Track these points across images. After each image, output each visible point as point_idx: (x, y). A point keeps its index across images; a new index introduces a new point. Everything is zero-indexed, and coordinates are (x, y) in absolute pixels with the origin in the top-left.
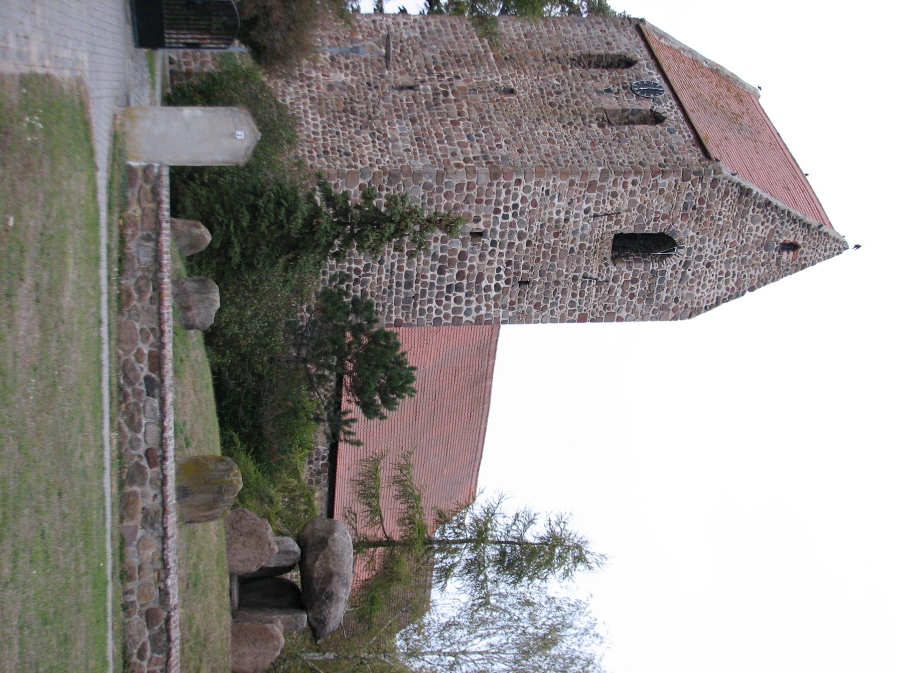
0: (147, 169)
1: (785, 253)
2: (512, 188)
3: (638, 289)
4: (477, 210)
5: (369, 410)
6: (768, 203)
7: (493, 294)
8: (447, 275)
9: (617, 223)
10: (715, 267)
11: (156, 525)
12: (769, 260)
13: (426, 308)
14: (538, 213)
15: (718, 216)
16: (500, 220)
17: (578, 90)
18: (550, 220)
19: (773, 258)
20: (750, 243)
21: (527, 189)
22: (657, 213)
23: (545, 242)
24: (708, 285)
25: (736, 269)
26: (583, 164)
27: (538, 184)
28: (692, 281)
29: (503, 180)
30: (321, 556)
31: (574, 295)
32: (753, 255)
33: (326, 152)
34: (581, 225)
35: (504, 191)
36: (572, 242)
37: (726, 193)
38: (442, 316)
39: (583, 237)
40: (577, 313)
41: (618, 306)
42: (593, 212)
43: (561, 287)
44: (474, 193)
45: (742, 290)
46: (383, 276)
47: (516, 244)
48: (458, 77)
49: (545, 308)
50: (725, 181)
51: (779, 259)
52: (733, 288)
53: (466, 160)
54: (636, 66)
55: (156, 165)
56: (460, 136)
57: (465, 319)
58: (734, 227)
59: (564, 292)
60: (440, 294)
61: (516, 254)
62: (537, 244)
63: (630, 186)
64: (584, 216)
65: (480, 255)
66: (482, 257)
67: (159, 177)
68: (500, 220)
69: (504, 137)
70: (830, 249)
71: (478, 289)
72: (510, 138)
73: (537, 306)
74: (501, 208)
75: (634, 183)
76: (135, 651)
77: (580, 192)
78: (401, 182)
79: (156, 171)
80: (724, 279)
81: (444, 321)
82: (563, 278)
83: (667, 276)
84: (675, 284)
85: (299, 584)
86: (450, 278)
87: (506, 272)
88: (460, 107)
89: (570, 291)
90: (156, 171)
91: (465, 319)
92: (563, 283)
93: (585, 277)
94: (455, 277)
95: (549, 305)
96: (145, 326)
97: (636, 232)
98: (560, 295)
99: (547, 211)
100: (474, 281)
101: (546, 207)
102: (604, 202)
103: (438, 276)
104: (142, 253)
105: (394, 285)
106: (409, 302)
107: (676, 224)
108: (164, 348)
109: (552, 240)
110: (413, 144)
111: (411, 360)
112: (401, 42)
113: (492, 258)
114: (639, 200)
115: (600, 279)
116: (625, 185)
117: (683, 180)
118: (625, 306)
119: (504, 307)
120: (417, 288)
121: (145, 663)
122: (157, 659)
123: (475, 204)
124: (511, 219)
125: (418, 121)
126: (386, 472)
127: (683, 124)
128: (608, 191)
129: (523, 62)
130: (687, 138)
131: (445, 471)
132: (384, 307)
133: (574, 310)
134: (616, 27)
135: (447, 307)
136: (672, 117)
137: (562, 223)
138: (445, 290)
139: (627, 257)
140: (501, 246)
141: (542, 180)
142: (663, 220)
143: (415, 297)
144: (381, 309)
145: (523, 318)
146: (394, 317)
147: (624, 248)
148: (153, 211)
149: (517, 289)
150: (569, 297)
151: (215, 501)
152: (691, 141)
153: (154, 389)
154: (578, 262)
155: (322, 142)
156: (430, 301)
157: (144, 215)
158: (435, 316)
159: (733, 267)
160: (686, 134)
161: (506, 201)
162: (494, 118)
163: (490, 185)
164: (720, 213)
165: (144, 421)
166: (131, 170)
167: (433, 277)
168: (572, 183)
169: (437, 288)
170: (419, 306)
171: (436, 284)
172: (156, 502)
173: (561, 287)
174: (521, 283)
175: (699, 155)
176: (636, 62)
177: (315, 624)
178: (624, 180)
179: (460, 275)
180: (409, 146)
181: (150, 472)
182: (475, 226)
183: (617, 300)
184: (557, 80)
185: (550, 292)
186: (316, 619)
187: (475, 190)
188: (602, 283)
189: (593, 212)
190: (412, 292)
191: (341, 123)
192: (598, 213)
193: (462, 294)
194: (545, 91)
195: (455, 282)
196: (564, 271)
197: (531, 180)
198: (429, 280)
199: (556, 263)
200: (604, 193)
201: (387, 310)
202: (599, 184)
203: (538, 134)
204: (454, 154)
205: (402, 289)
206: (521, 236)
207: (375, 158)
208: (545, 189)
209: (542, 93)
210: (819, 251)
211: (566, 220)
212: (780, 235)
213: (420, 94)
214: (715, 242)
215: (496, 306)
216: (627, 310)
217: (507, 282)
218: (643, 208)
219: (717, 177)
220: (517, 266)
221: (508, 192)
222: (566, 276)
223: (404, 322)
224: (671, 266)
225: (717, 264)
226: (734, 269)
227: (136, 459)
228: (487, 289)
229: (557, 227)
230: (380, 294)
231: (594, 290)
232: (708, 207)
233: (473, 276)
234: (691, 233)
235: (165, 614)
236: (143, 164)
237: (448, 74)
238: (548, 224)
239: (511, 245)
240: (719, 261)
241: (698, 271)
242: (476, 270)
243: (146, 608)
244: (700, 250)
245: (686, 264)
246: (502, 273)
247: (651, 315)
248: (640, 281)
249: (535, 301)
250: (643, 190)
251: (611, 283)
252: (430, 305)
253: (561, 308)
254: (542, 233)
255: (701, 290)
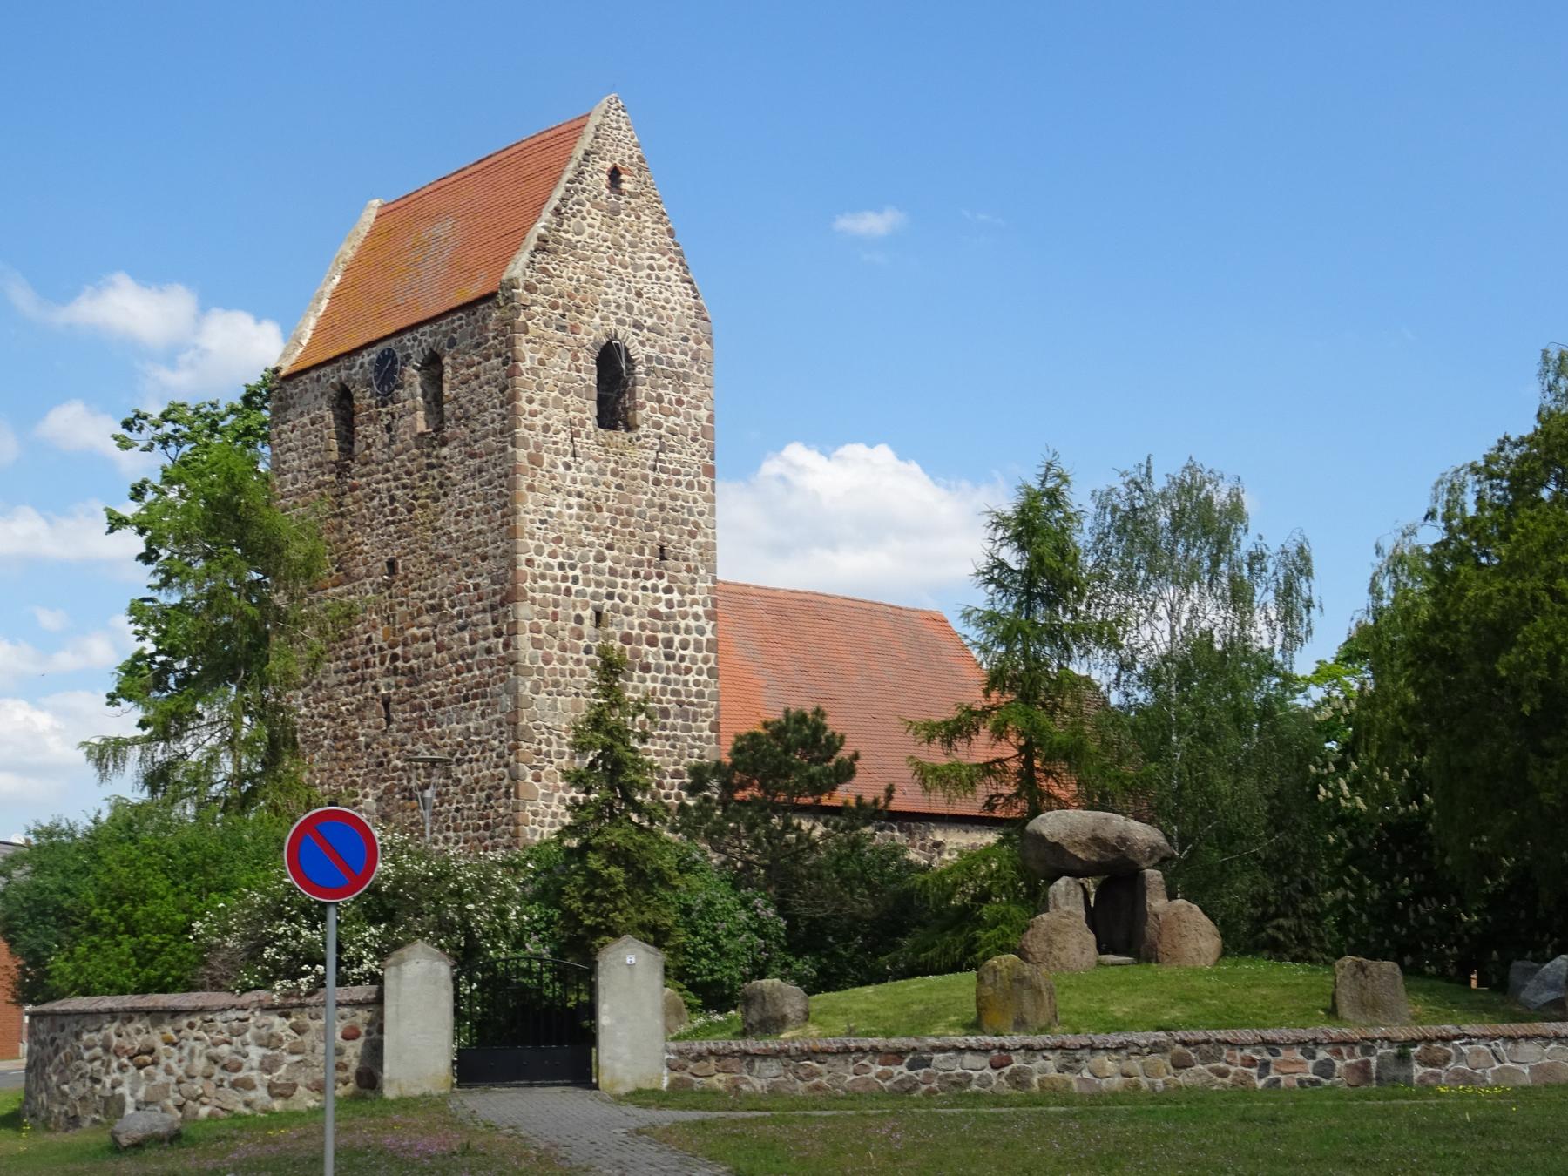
0: (672, 1067)
1: (624, 186)
2: (537, 571)
3: (670, 394)
4: (567, 619)
5: (846, 772)
6: (557, 211)
7: (676, 596)
8: (651, 660)
9: (583, 424)
10: (641, 285)
11: (1078, 1056)
12: (633, 209)
13: (694, 689)
14: (570, 536)
15: (574, 283)
16: (579, 587)
17: (387, 471)
18: (579, 518)
19: (629, 203)
20: (610, 236)
21: (539, 551)
22: (570, 369)
23: (608, 524)
24: (666, 294)
25: (645, 256)
26: (502, 472)
27: (532, 536)
28: (660, 318)
29: (527, 584)
30: (1071, 851)
31: (679, 484)
32: (626, 231)
33: (487, 827)
34: (585, 475)
35: (541, 582)
36: (609, 487)
37: (544, 270)
38: (705, 667)
39: (602, 472)
40: (702, 479)
41: (693, 422)
42: (569, 459)
43: (668, 502)
44: (544, 624)
45: (673, 247)
46: (653, 748)
47: (611, 564)
48: (369, 640)
49: (696, 524)
50: (528, 273)
51: (631, 195)
52: (670, 260)
53: (498, 634)
54: (350, 385)
55: (667, 1056)
56: (462, 640)
57: (709, 635)
58: (588, 259)
59: (674, 497)
60: (677, 670)
61: (623, 564)
62: (610, 535)
63: (535, 406)
64: (573, 470)
65: (626, 614)
66: (628, 612)
67: (679, 1053)
68: (579, 587)
69: (461, 580)
70: (617, 122)
71: (670, 617)
72: (462, 573)
73: (692, 535)
74: (563, 586)
75: (530, 401)
76: (1219, 1080)
77: (543, 476)
78: (531, 724)
79: (673, 1057)
80: (657, 272)
81: (712, 664)
82: (656, 500)
83: (654, 352)
84: (664, 341)
85: (1101, 878)
86: (656, 655)
87: (647, 578)
88: (415, 638)
89: (674, 489)
90: (673, 1057)
91: (709, 635)
92: (662, 500)
93: (654, 469)
94: (654, 649)
95: (692, 518)
96: (851, 1069)
97: (595, 397)
98: (679, 503)
99: (568, 522)
100: (659, 623)
101: (563, 524)
102: (555, 443)
103: (653, 673)
104: (767, 1073)
105: (664, 733)
106: (687, 712)
107: (585, 341)
108: (876, 1047)
109: (606, 514)
110: (473, 707)
111: (776, 715)
112: (312, 717)
113: (630, 598)
114: (553, 394)
115: (657, 447)
116: (533, 414)
117: (526, 332)
118: (692, 412)
119: (693, 581)
120: (669, 702)
121: (1233, 1069)
122: (1228, 1055)
123: (558, 622)
124: (578, 572)
125: (438, 697)
126: (936, 755)
127: (441, 326)
128: (541, 438)
129: (344, 546)
130: (463, 322)
131: (903, 656)
132: (693, 747)
133: (699, 482)
134: (286, 409)
135: (694, 660)
136: (430, 340)
137: (584, 501)
138: (671, 663)
139: (625, 410)
140: (613, 585)
141: (527, 530)
142: (578, 360)
143: (680, 704)
144: (696, 751)
145: (708, 552)
146: (707, 733)
147: (614, 412)
148: (718, 1061)
149: (670, 563)
150: (682, 490)
151: (1031, 987)
152: (468, 316)
153: (923, 1060)
154: (634, 478)
155: (471, 833)
156: (686, 683)
157: (724, 1070)
158: (705, 677)
159: (641, 259)
160: (457, 324)
161: (554, 579)
162: (431, 591)
163: (533, 601)
164: (570, 279)
165: (960, 1071)
166: (674, 1084)
167: (654, 680)
168: (531, 488)
169: (668, 673)
170: (693, 699)
171: (664, 675)
172: (1051, 1057)
173: (668, 502)
174: (663, 558)
175: (490, 308)
176: (342, 384)
177: (1156, 860)
178: (526, 416)
179: (652, 642)
180: (478, 711)
181: (1018, 1062)
182: (587, 622)
183: (685, 423)
184: (372, 499)
185: (674, 517)
186: (1150, 858)
187: (540, 622)
188: (663, 444)
189: (569, 459)
190: (673, 708)
191: (441, 805)
192: (570, 450)
193: (677, 639)
194: (390, 518)
195: (661, 648)
196: (646, 497)
197: (527, 545)
198: (659, 686)
199: (637, 509)
200: (544, 442)
201: (698, 743)
202: (532, 450)
203: (456, 531)
204: (489, 651)
205: (670, 721)
206: (600, 558)
207: (495, 759)
208: (539, 525)
209: (393, 522)
210: (620, 137)
211: (580, 495)
212: (600, 194)
213: (395, 694)
214: (609, 286)
215: (692, 592)
216: (698, 408)
217: (660, 576)
218: (563, 389)
219: (522, 284)
220: (640, 563)
221: (543, 577)
222: (654, 494)
223: (713, 719)
224: (640, 347)
225: (637, 283)
226: (643, 258)
227: (1003, 1080)
228: (669, 604)
229: (588, 508)
230: (676, 752)
231: (671, 455)
232: (561, 296)
233: (653, 624)
234: (597, 320)
235: (1179, 1047)
236: (666, 1071)
237: (363, 653)
238: (585, 521)
239: (612, 572)
240: (633, 279)
241: (648, 310)
242: (645, 620)
243: (1171, 1068)
244: (618, 306)
245: (638, 326)
246: (649, 584)
247: (705, 375)
248: (660, 391)
249: (686, 537)
250: (540, 388)
251: (662, 432)
252: (691, 684)
253: (695, 501)
254: (597, 529)
255: (672, 305)
